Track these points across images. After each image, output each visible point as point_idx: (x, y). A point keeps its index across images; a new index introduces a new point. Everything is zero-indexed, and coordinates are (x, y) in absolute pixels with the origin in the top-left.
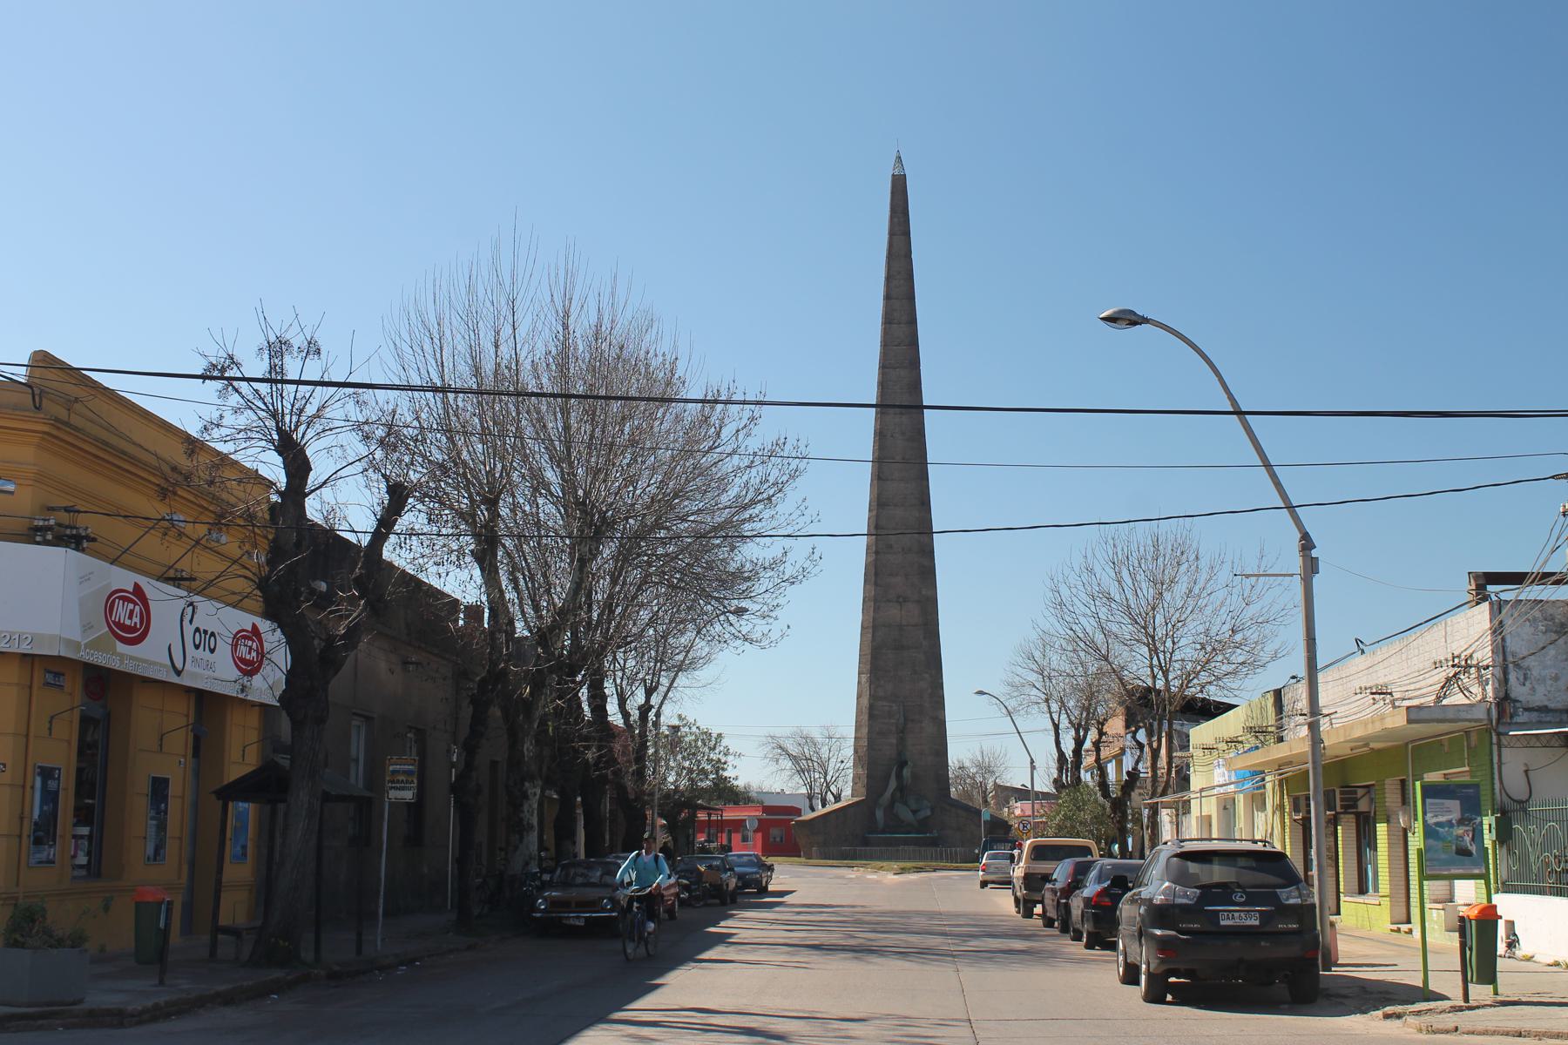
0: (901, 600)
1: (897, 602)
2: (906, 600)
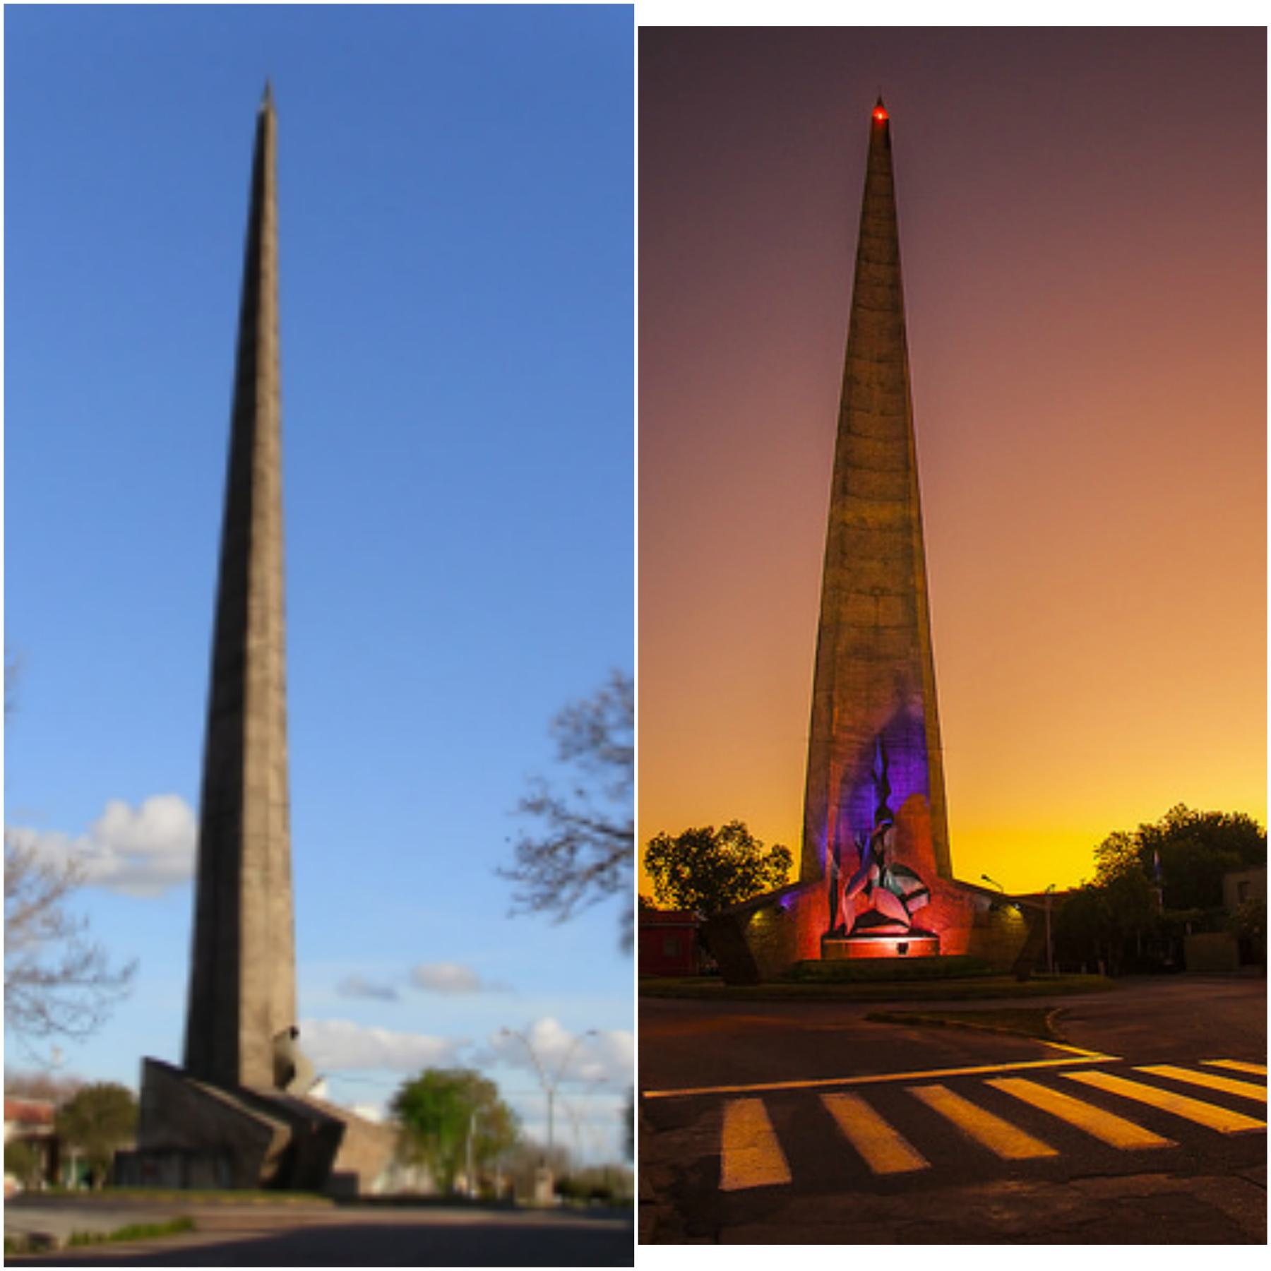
0: (877, 592)
1: (871, 595)
2: (884, 592)
